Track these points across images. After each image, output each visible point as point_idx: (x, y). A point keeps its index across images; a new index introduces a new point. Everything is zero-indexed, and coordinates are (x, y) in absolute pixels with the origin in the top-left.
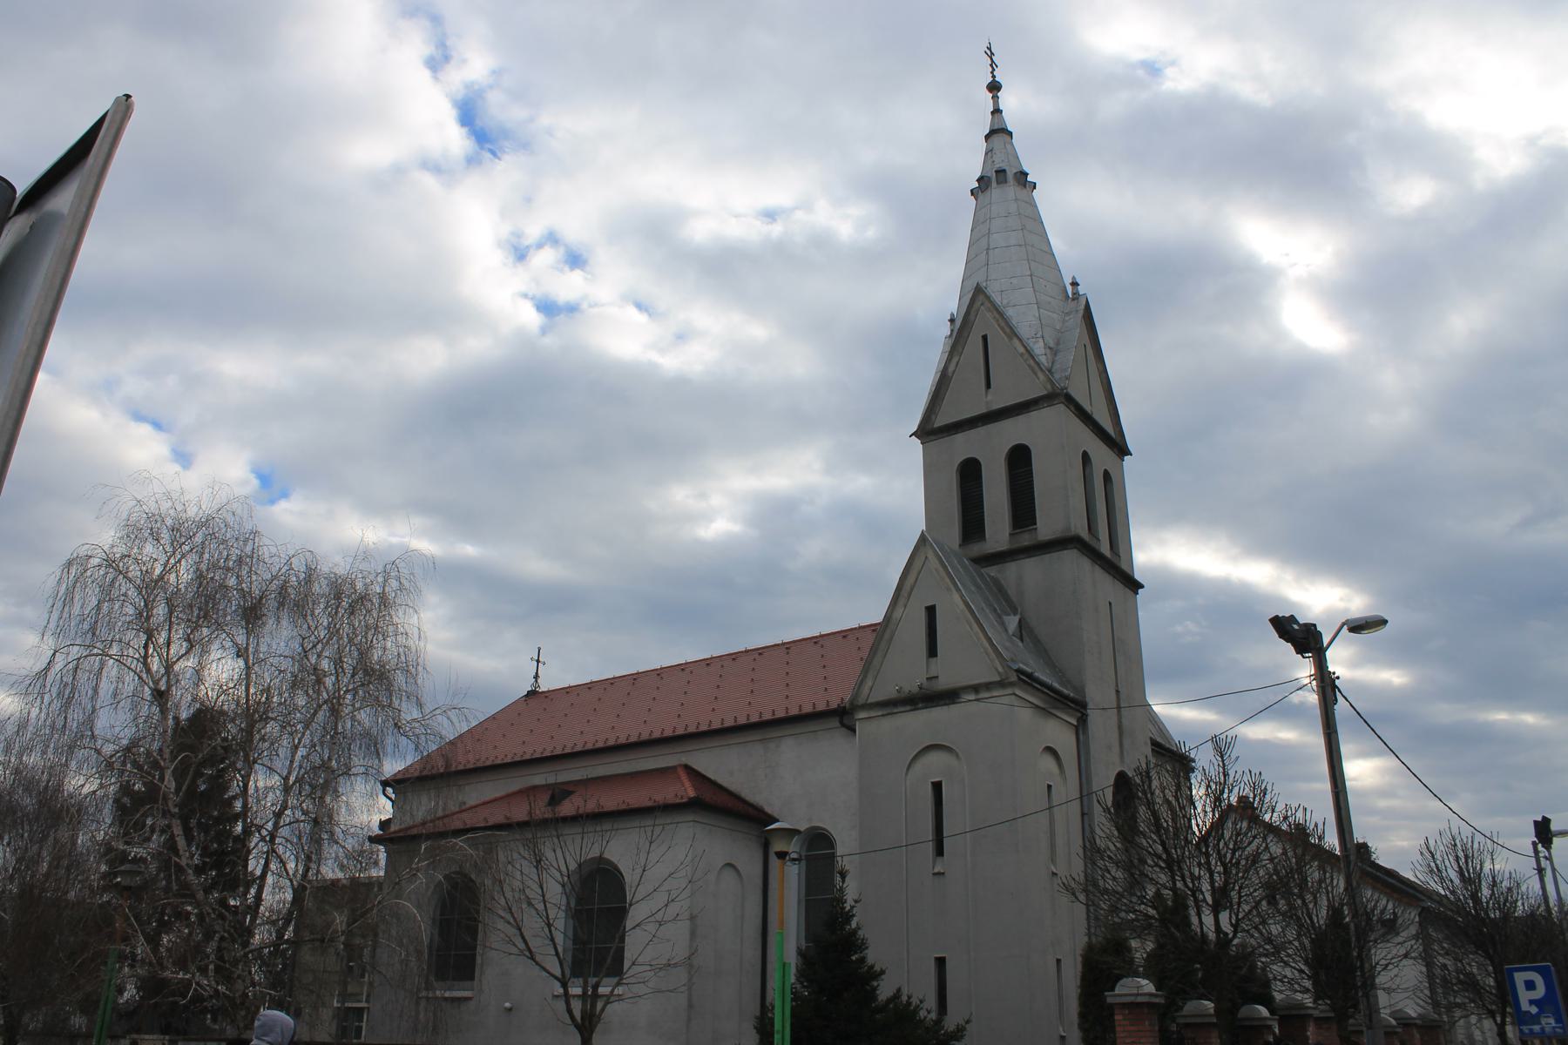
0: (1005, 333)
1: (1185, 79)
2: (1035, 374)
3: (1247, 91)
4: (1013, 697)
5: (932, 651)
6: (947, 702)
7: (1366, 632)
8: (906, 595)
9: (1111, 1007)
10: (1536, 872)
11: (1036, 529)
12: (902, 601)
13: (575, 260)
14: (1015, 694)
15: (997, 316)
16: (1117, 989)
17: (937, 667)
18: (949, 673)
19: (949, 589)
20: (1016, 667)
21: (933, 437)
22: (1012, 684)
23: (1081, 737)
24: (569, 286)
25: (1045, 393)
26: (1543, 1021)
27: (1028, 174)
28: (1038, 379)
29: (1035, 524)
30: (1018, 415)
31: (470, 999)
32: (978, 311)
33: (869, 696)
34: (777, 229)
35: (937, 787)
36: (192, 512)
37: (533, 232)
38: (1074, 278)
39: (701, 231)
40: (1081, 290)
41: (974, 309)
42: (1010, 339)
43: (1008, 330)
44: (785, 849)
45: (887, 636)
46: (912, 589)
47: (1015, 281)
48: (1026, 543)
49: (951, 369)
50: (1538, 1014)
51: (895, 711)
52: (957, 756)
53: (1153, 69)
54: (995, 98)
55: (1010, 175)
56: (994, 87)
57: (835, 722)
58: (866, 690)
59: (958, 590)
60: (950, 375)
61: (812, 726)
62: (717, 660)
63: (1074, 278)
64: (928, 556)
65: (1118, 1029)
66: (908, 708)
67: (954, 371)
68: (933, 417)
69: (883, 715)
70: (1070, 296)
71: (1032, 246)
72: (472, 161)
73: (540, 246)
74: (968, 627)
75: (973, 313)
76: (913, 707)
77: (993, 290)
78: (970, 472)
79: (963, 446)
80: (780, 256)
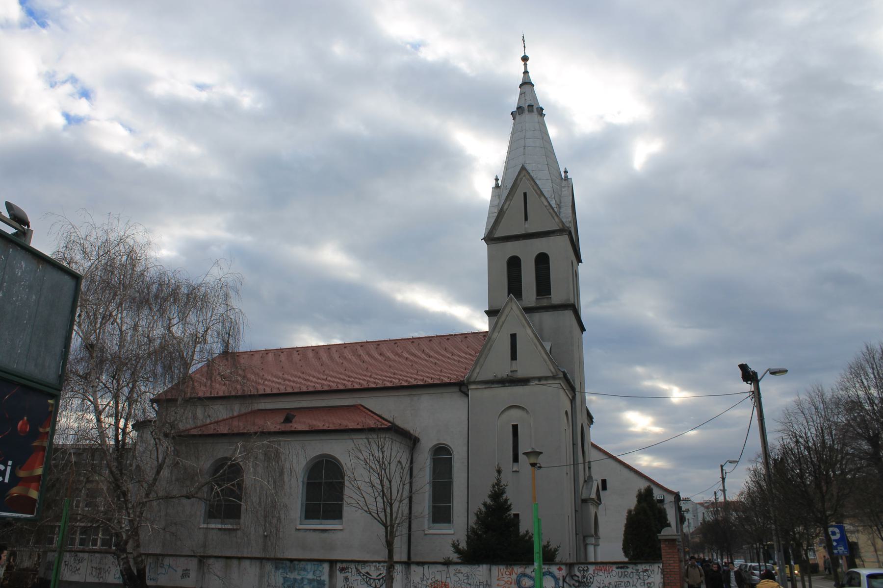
1: (429, 55)
2: (553, 218)
3: (463, 66)
4: (559, 385)
5: (514, 357)
6: (522, 384)
9: (660, 541)
10: (721, 479)
11: (551, 297)
12: (497, 329)
13: (85, 94)
14: (560, 383)
15: (533, 184)
16: (662, 532)
17: (516, 365)
18: (523, 369)
19: (524, 326)
20: (562, 370)
21: (493, 242)
23: (573, 406)
24: (82, 107)
25: (558, 228)
26: (839, 548)
28: (554, 220)
29: (550, 295)
32: (522, 179)
34: (203, 96)
35: (515, 428)
37: (61, 76)
38: (565, 169)
39: (159, 89)
40: (569, 176)
41: (519, 178)
42: (540, 197)
44: (535, 462)
45: (488, 347)
46: (503, 323)
47: (539, 166)
48: (545, 304)
49: (505, 207)
50: (837, 546)
51: (493, 386)
52: (527, 412)
53: (416, 46)
54: (525, 65)
55: (535, 108)
56: (525, 59)
57: (456, 389)
58: (475, 375)
59: (530, 327)
60: (505, 210)
61: (431, 391)
62: (333, 346)
63: (565, 169)
65: (663, 551)
66: (500, 385)
67: (507, 209)
68: (494, 231)
69: (485, 388)
70: (563, 178)
71: (547, 148)
72: (24, 26)
73: (65, 82)
74: (535, 347)
75: (519, 180)
76: (503, 385)
78: (514, 264)
80: (206, 111)
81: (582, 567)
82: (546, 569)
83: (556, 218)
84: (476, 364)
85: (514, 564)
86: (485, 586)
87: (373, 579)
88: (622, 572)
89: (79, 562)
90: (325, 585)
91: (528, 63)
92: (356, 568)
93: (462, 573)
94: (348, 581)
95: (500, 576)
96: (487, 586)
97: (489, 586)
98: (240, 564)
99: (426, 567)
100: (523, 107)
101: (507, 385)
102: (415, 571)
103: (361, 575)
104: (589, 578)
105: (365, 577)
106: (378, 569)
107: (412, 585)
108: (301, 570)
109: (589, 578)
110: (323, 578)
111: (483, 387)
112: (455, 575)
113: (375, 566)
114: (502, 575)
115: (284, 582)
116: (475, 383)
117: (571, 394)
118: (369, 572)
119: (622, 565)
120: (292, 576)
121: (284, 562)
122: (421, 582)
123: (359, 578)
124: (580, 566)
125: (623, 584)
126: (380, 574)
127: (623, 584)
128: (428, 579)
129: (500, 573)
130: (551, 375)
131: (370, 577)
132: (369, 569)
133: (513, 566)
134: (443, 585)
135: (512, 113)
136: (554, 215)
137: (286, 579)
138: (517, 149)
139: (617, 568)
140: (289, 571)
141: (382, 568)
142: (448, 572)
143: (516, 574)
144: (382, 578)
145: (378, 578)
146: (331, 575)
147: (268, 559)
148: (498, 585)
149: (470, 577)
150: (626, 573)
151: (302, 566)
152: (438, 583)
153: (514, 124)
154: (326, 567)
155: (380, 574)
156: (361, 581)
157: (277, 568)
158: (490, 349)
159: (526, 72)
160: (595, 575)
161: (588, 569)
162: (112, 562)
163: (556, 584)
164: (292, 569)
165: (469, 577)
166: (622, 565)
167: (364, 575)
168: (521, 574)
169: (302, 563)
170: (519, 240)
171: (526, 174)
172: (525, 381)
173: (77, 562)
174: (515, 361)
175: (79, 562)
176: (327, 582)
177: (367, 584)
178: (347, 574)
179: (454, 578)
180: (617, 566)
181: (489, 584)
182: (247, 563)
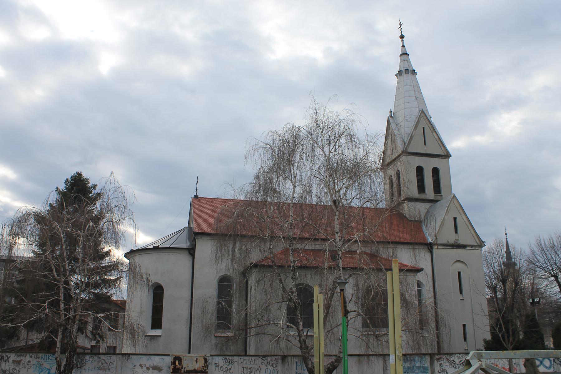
0: (430, 130)
5: (456, 232)
6: (463, 248)
7: (461, 248)
25: (444, 154)
30: (435, 158)
32: (421, 118)
35: (459, 273)
36: (331, 120)
43: (432, 129)
49: (413, 134)
54: (402, 41)
57: (426, 247)
66: (451, 248)
67: (414, 135)
76: (452, 248)
83: (442, 148)
87: (456, 364)
89: (229, 364)
90: (428, 369)
92: (446, 358)
94: (442, 366)
98: (369, 359)
100: (402, 71)
101: (454, 248)
103: (450, 362)
110: (426, 365)
113: (457, 356)
116: (438, 245)
123: (448, 364)
126: (461, 361)
130: (477, 245)
131: (455, 363)
138: (410, 96)
141: (462, 357)
144: (462, 363)
145: (460, 363)
146: (432, 363)
154: (428, 358)
155: (461, 361)
156: (450, 366)
159: (403, 46)
162: (262, 363)
163: (550, 363)
167: (451, 362)
170: (423, 157)
172: (464, 247)
173: (228, 364)
175: (229, 364)
176: (430, 368)
178: (441, 362)
182: (373, 358)
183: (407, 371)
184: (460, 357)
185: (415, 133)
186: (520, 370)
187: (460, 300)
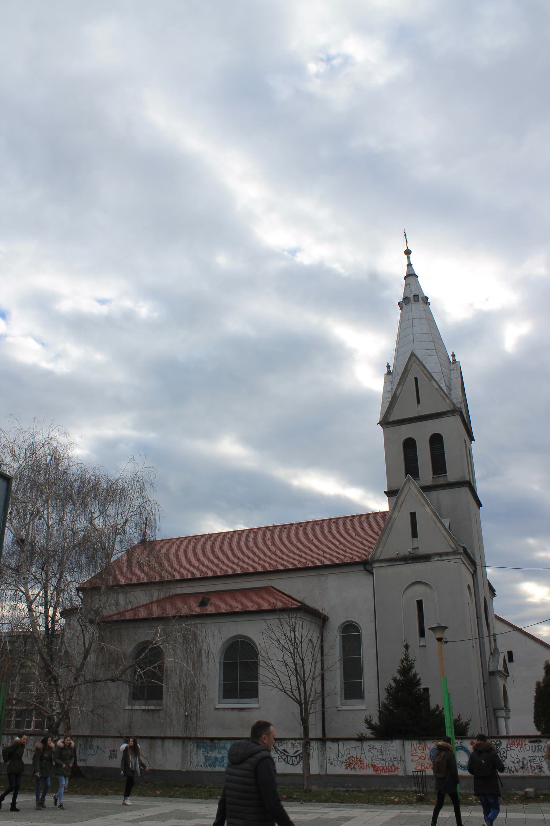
2: (444, 400)
4: (460, 560)
5: (415, 534)
6: (425, 560)
7: (422, 560)
8: (399, 506)
11: (447, 476)
12: (397, 509)
15: (423, 369)
17: (417, 543)
20: (462, 545)
21: (389, 426)
22: (460, 554)
25: (450, 409)
27: (428, 298)
28: (446, 401)
29: (446, 473)
31: (160, 710)
33: (380, 556)
35: (420, 603)
38: (453, 352)
40: (457, 358)
42: (430, 381)
43: (429, 376)
44: (441, 637)
47: (428, 351)
48: (441, 483)
49: (398, 392)
51: (396, 564)
52: (431, 587)
54: (408, 258)
56: (408, 252)
57: (361, 568)
58: (378, 553)
59: (429, 505)
61: (346, 569)
63: (453, 352)
64: (411, 488)
66: (403, 563)
67: (399, 394)
68: (389, 415)
69: (389, 566)
70: (451, 361)
75: (409, 366)
76: (406, 562)
77: (418, 354)
79: (407, 431)
81: (494, 742)
82: (459, 743)
84: (379, 543)
85: (427, 739)
86: (399, 762)
87: (290, 756)
88: (535, 746)
91: (410, 256)
93: (376, 749)
95: (414, 751)
96: (402, 762)
97: (403, 761)
99: (341, 743)
101: (410, 562)
102: (330, 748)
103: (279, 752)
104: (502, 752)
105: (282, 754)
106: (294, 746)
107: (328, 761)
108: (221, 748)
109: (502, 752)
111: (387, 565)
112: (369, 751)
113: (292, 743)
114: (416, 750)
115: (206, 761)
116: (379, 561)
117: (472, 568)
118: (286, 749)
119: (535, 739)
120: (214, 754)
121: (205, 741)
122: (336, 759)
124: (492, 740)
125: (537, 759)
126: (297, 751)
127: (537, 759)
128: (343, 755)
129: (413, 748)
130: (451, 550)
131: (287, 754)
132: (286, 746)
133: (426, 741)
134: (358, 762)
135: (399, 304)
136: (445, 397)
137: (207, 758)
138: (406, 336)
139: (530, 742)
140: (210, 749)
142: (362, 748)
143: (429, 749)
144: (299, 755)
147: (190, 739)
148: (412, 761)
149: (384, 753)
150: (540, 747)
151: (222, 745)
152: (353, 759)
153: (402, 314)
155: (297, 751)
156: (279, 759)
157: (198, 747)
158: (392, 527)
159: (409, 265)
160: (509, 749)
161: (500, 744)
164: (213, 748)
165: (383, 752)
166: (535, 739)
167: (281, 753)
168: (434, 749)
169: (222, 741)
171: (416, 360)
172: (426, 558)
174: (422, 639)
177: (285, 761)
179: (368, 754)
180: (530, 740)
181: (403, 759)
182: (169, 744)
183: (214, 764)
184: (297, 744)
185: (402, 389)
186: (405, 770)
187: (419, 646)
